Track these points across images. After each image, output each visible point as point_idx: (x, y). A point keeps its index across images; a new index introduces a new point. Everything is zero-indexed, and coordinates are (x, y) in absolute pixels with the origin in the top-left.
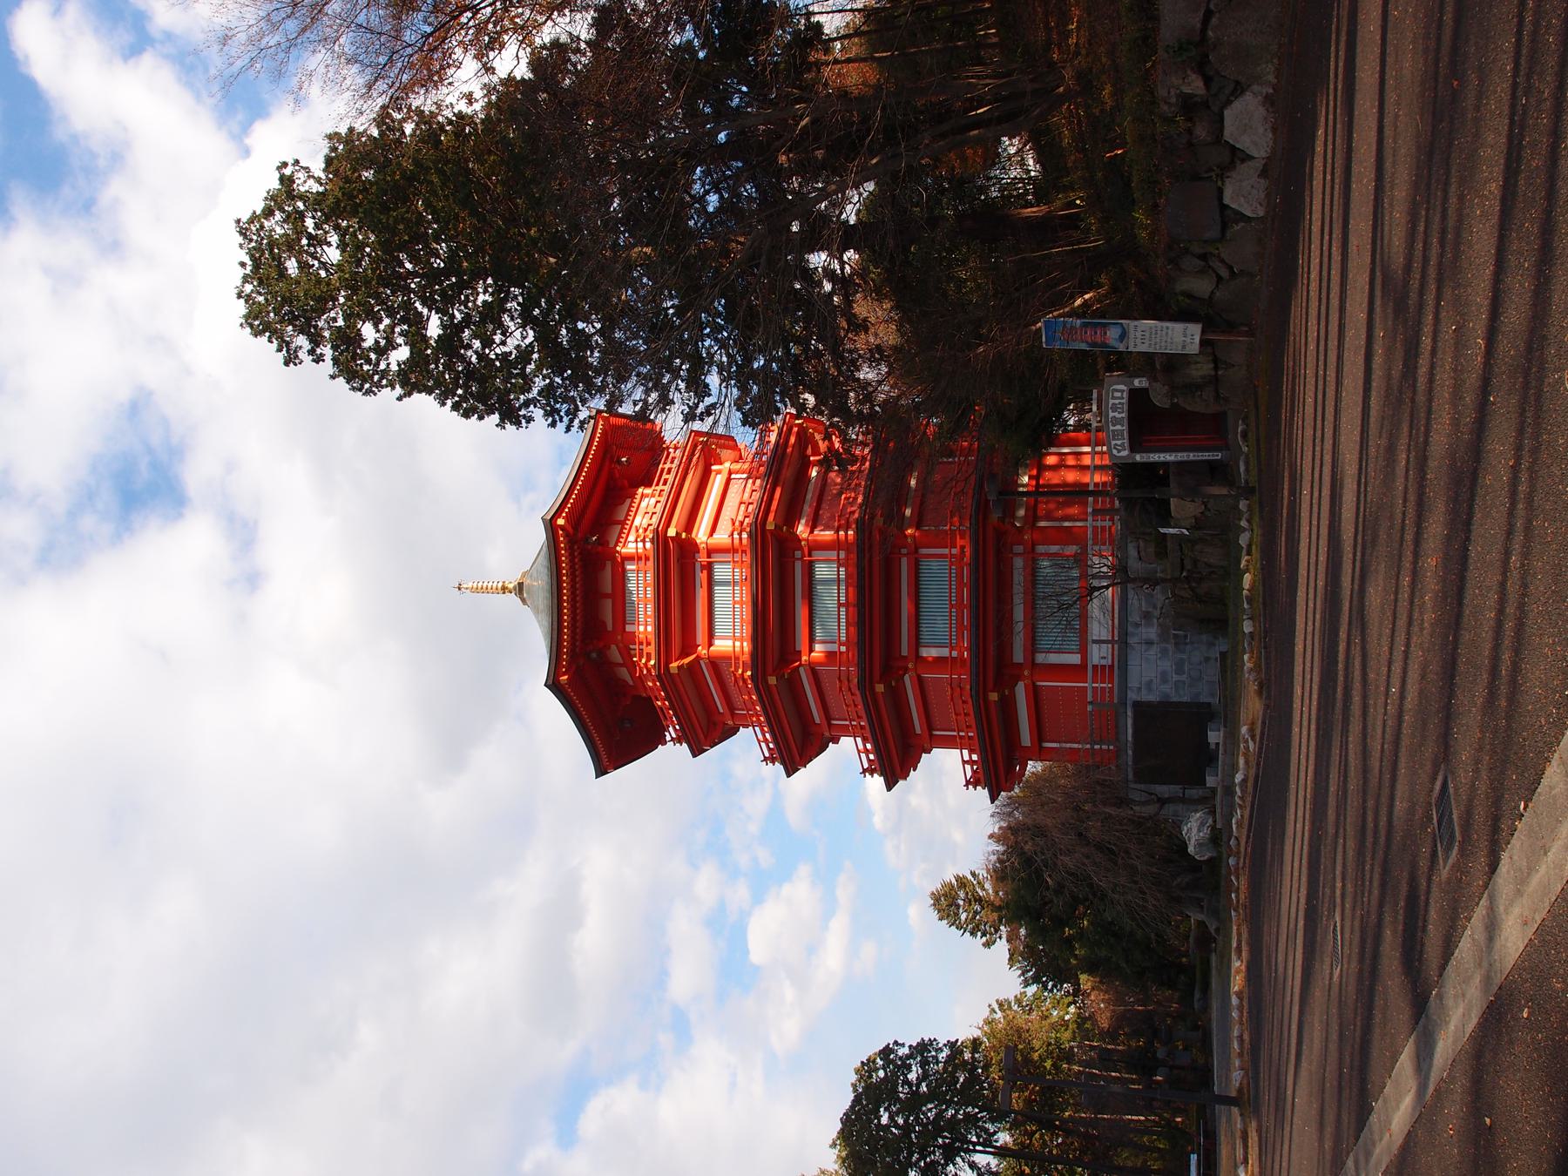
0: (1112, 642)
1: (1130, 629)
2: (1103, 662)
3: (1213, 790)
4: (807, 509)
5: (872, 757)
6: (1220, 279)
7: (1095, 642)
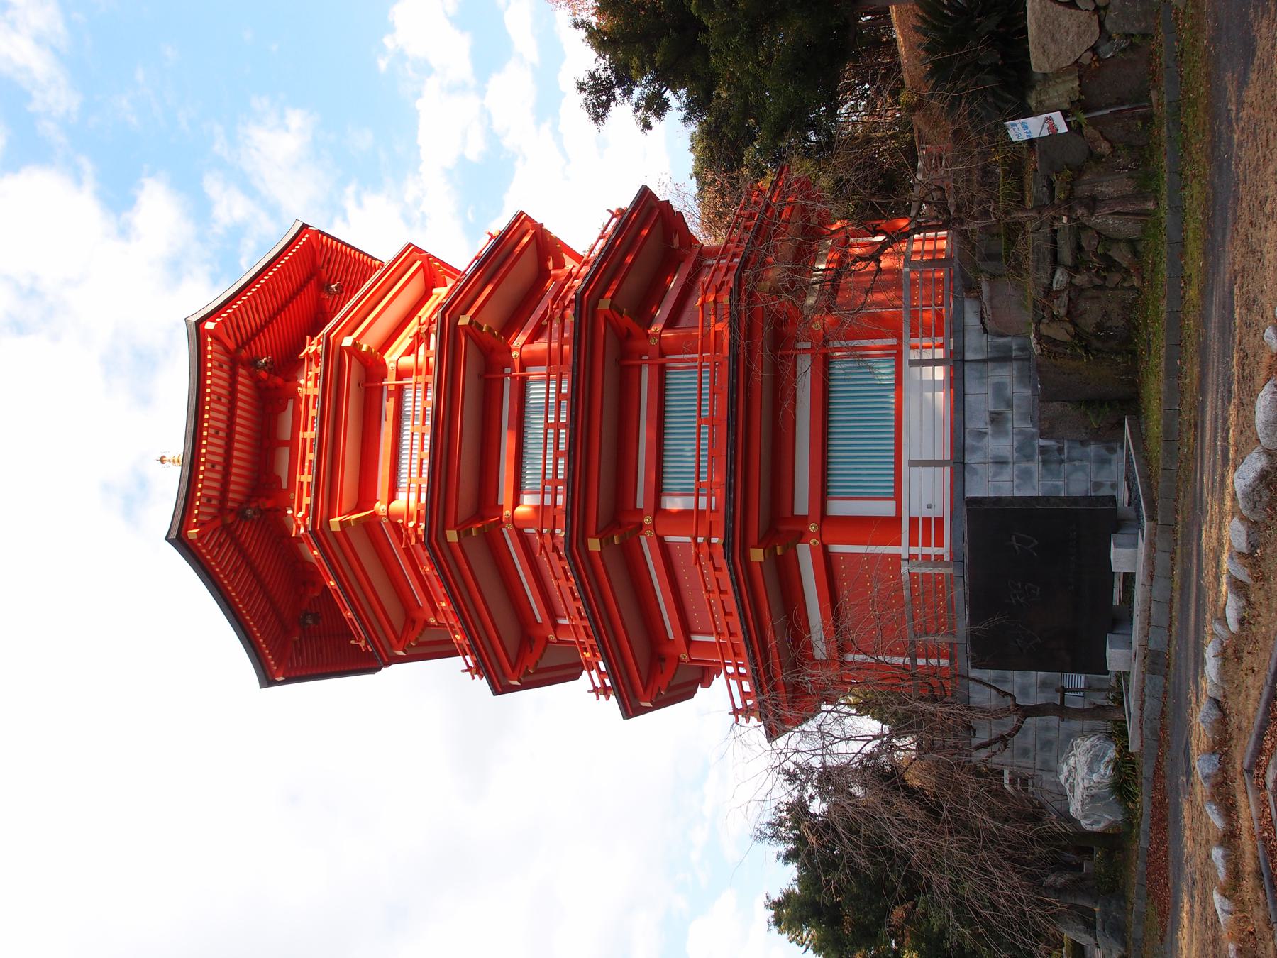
1: (969, 441)
2: (927, 513)
3: (1123, 677)
4: (533, 321)
5: (747, 687)
7: (913, 463)
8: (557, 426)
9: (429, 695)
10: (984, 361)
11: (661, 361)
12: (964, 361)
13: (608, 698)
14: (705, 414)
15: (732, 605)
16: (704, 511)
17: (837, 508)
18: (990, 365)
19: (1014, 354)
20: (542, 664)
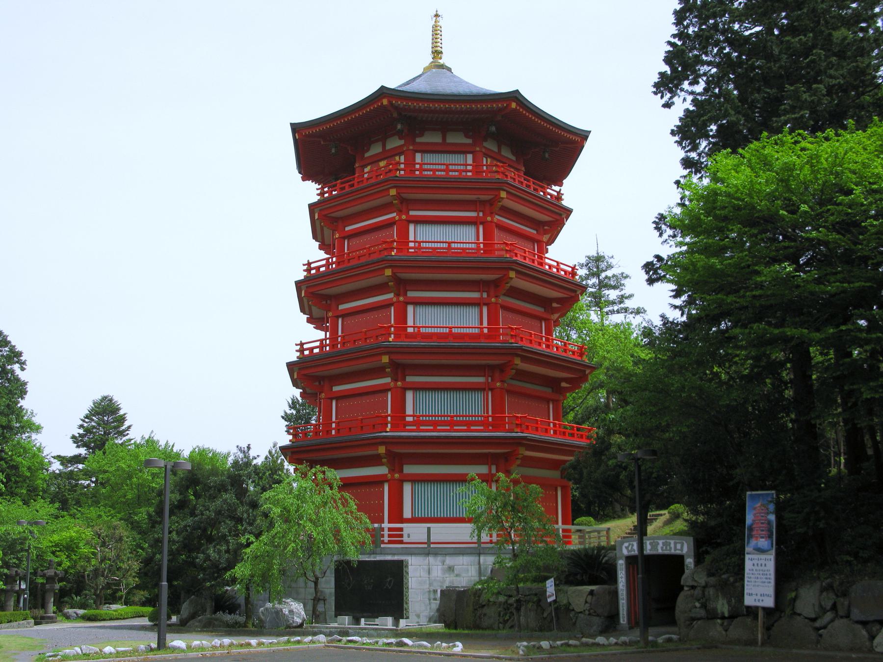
0: (429, 542)
2: (405, 533)
5: (316, 351)
6: (814, 620)
7: (429, 529)
8: (447, 170)
12: (479, 554)
13: (318, 195)
14: (453, 245)
15: (363, 260)
17: (407, 488)
20: (325, 229)
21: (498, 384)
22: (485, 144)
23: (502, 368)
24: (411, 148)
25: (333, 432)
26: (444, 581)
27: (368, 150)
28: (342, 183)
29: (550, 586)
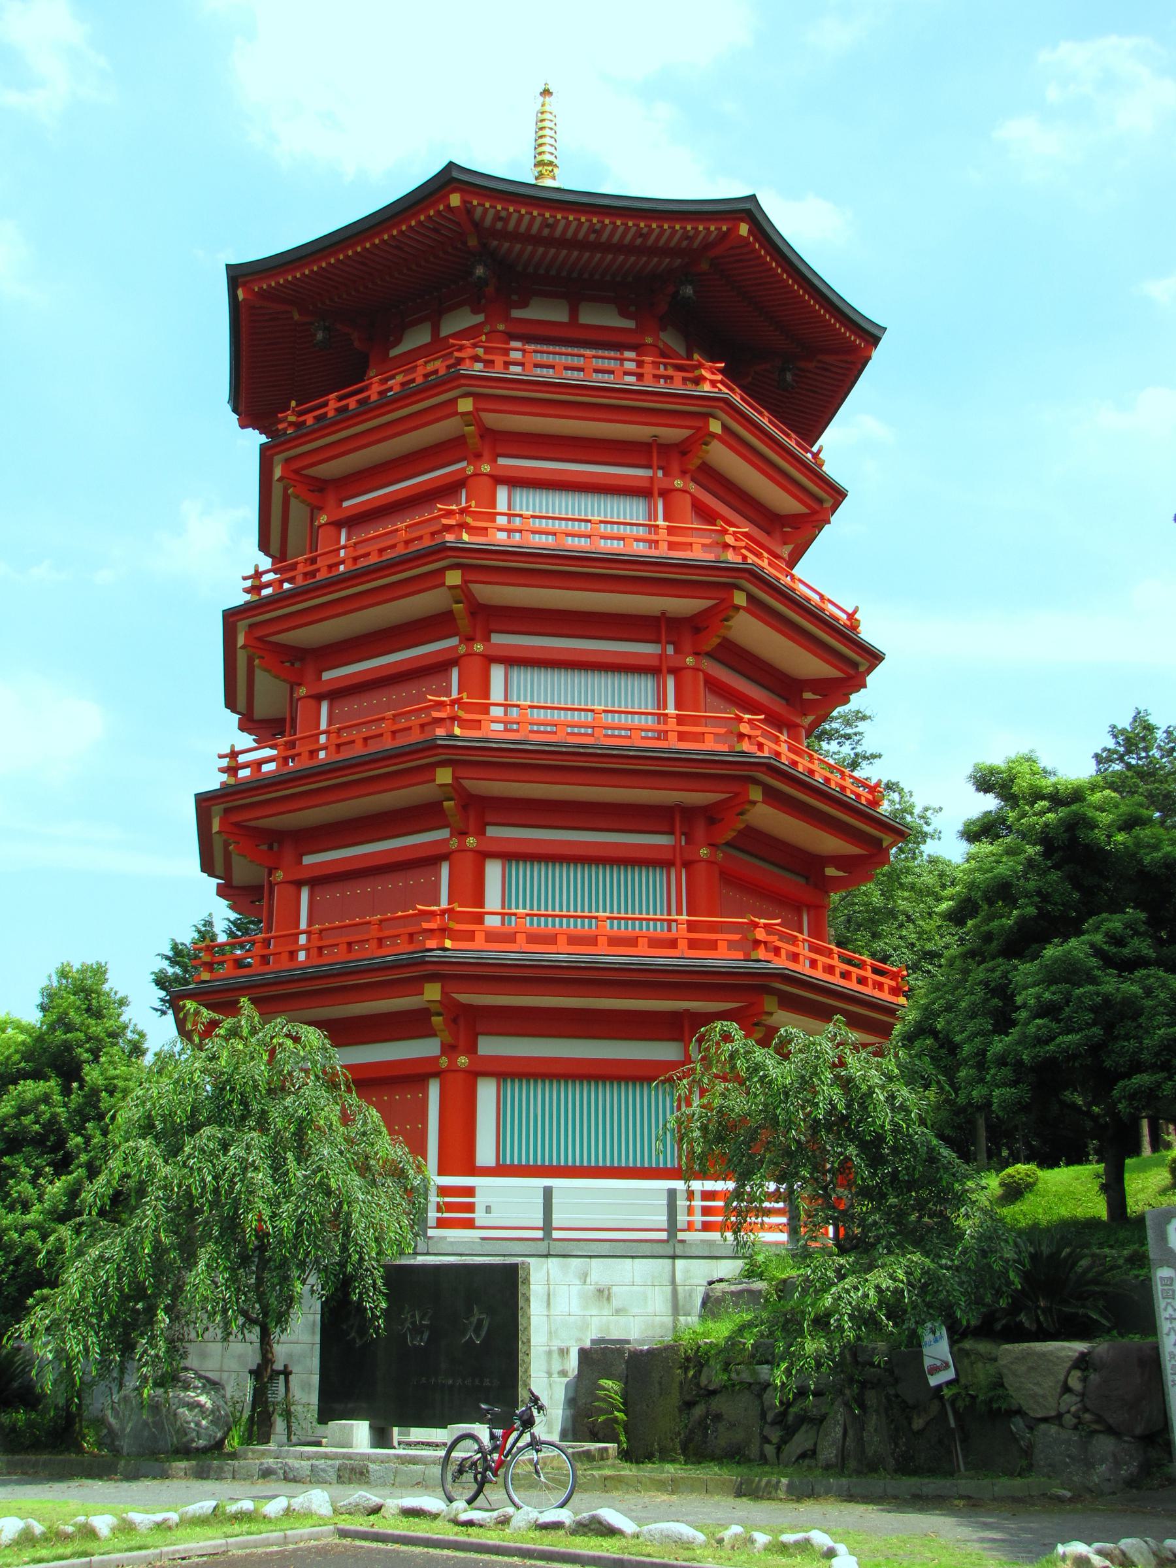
2: (479, 1200)
7: (548, 1193)
9: (208, 532)
10: (673, 1282)
11: (678, 861)
13: (247, 591)
16: (508, 355)
17: (486, 1092)
18: (669, 1289)
19: (681, 1318)
21: (704, 852)
22: (662, 335)
23: (711, 815)
24: (501, 327)
25: (302, 956)
26: (585, 1326)
27: (398, 341)
28: (340, 399)
29: (937, 1348)
